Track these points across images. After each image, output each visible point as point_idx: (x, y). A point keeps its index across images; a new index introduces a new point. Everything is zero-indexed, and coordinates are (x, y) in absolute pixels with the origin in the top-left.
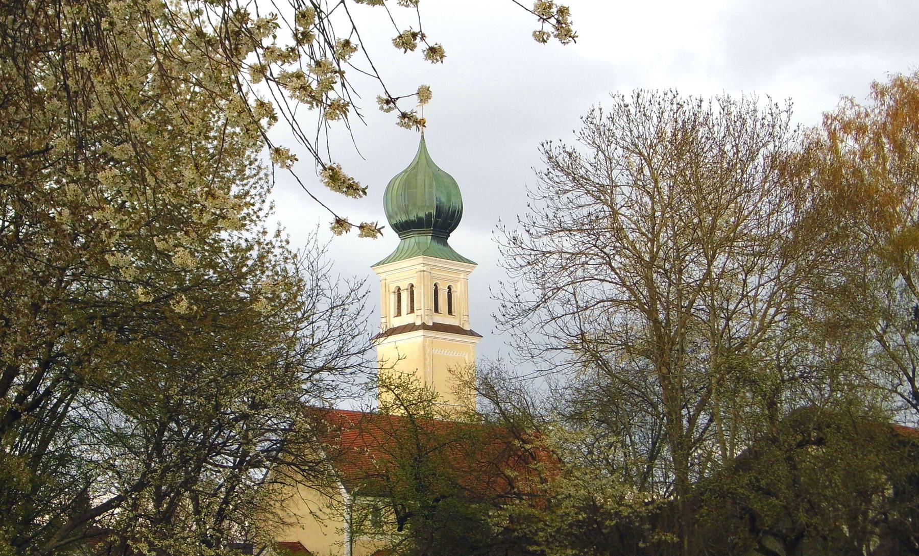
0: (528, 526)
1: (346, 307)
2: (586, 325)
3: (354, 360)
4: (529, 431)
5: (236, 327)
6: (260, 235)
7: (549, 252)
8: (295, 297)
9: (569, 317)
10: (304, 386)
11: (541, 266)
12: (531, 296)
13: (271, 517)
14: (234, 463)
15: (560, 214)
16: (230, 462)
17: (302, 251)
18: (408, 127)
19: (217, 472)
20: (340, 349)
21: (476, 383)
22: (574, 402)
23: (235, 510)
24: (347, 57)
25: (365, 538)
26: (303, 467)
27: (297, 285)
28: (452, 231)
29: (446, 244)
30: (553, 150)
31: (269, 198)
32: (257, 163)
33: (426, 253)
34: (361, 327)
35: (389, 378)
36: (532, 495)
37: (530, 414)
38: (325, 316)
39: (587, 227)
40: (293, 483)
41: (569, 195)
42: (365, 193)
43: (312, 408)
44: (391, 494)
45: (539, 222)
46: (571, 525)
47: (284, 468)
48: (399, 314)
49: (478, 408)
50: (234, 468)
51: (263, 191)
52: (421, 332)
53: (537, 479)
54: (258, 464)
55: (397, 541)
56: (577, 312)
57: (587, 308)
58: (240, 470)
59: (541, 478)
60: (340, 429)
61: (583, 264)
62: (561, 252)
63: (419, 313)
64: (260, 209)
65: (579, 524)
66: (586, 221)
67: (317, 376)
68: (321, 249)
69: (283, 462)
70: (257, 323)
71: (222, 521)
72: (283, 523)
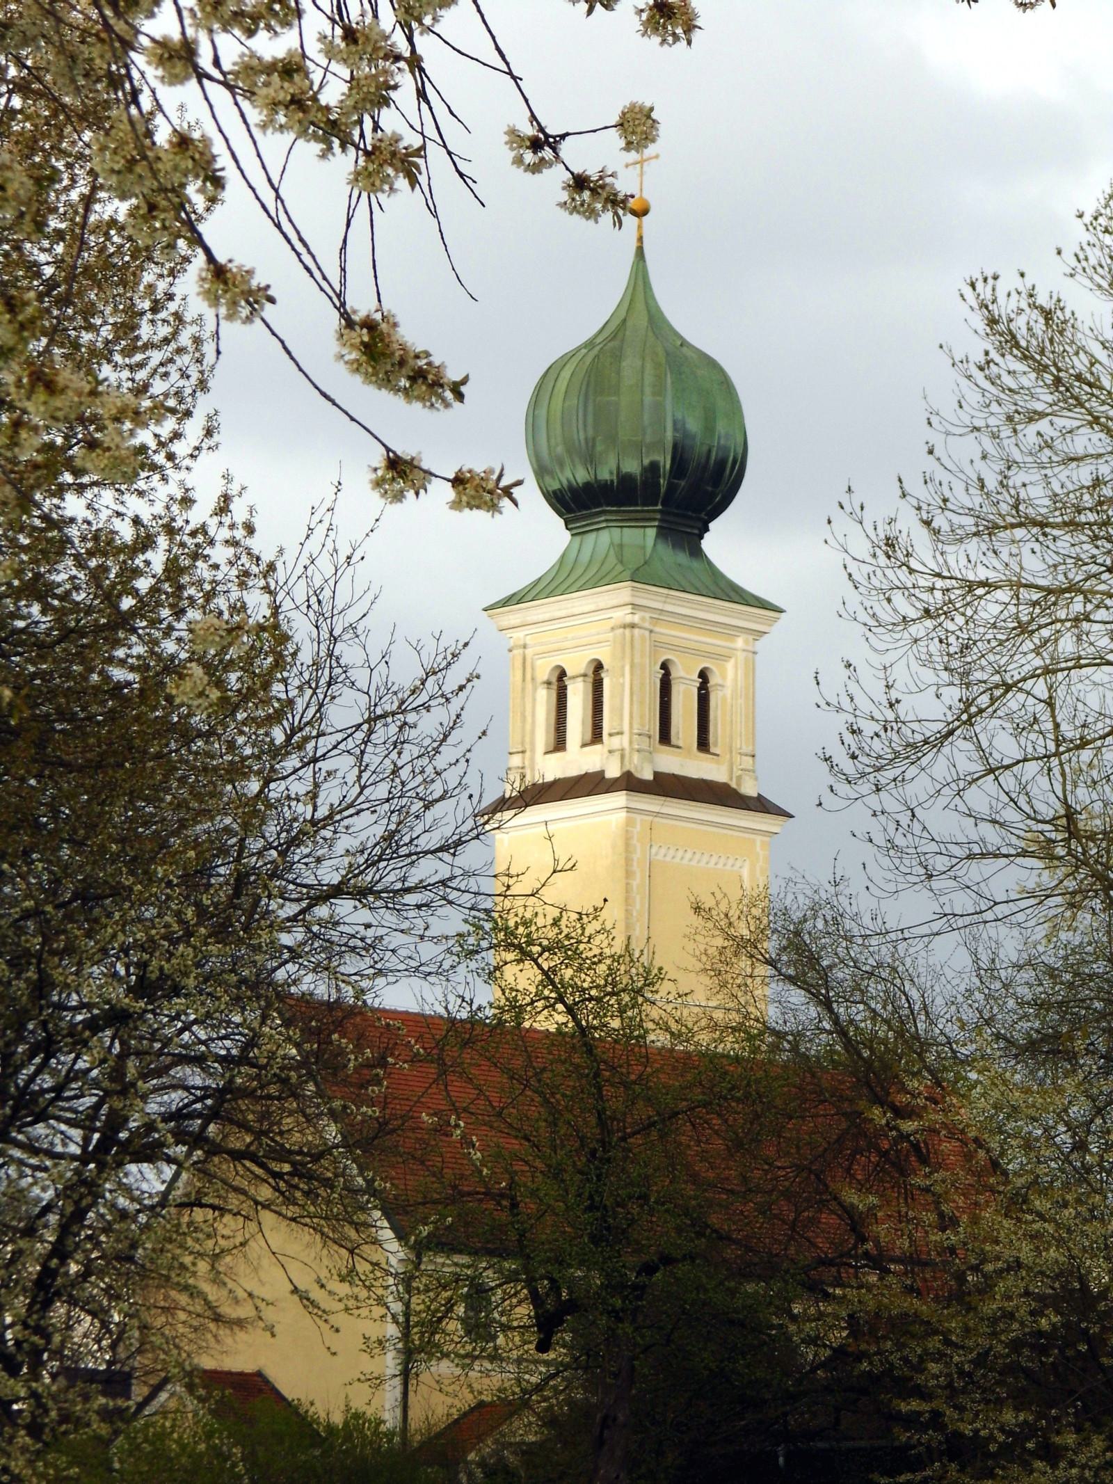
0: (900, 1346)
1: (411, 717)
2: (1082, 792)
3: (427, 869)
4: (913, 1084)
5: (99, 766)
6: (175, 509)
7: (984, 584)
8: (266, 686)
9: (1032, 768)
10: (286, 939)
11: (960, 620)
12: (930, 705)
13: (183, 1299)
14: (84, 1147)
15: (1017, 478)
16: (72, 1141)
17: (289, 556)
18: (591, 214)
19: (35, 1168)
20: (389, 837)
21: (771, 946)
22: (1042, 1005)
23: (84, 1276)
24: (427, 20)
25: (445, 1368)
26: (275, 1166)
27: (273, 651)
28: (715, 514)
29: (697, 552)
30: (1002, 299)
31: (203, 407)
32: (172, 306)
33: (641, 575)
34: (452, 777)
35: (526, 923)
36: (914, 1261)
37: (916, 1037)
38: (350, 744)
39: (1092, 517)
40: (247, 1207)
41: (1043, 425)
42: (460, 396)
43: (306, 1000)
44: (521, 1250)
45: (960, 497)
46: (1016, 1346)
47: (223, 1167)
48: (559, 743)
49: (773, 1014)
50: (84, 1159)
51: (188, 386)
52: (619, 799)
53: (930, 1217)
54: (149, 1153)
55: (534, 1379)
56: (1057, 754)
57: (1084, 743)
58: (101, 1166)
59: (941, 1215)
60: (382, 1062)
61: (1076, 620)
62: (1017, 585)
63: (615, 743)
64: (177, 435)
65: (1039, 1342)
66: (1088, 500)
67: (322, 911)
68: (344, 552)
69: (214, 1149)
70: (158, 756)
71: (47, 1304)
72: (218, 1318)
